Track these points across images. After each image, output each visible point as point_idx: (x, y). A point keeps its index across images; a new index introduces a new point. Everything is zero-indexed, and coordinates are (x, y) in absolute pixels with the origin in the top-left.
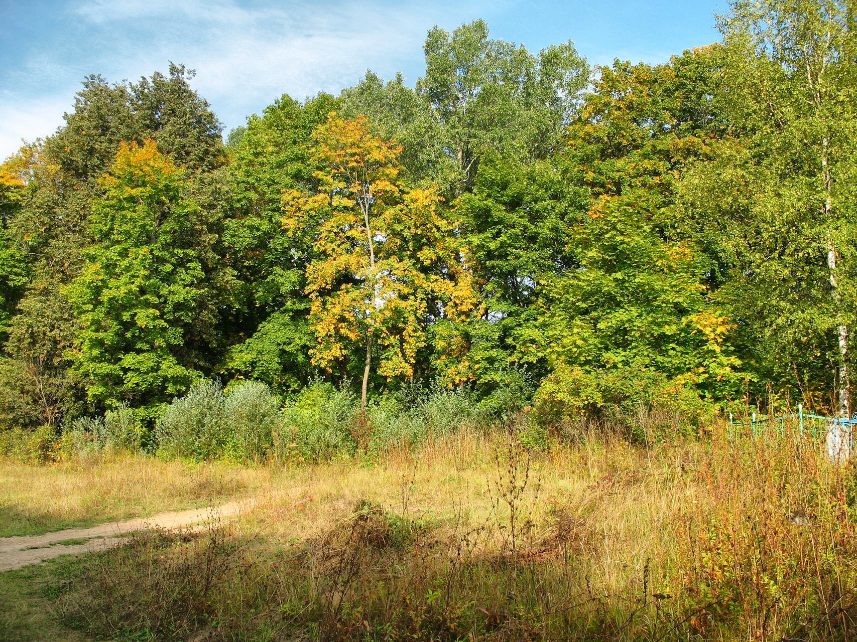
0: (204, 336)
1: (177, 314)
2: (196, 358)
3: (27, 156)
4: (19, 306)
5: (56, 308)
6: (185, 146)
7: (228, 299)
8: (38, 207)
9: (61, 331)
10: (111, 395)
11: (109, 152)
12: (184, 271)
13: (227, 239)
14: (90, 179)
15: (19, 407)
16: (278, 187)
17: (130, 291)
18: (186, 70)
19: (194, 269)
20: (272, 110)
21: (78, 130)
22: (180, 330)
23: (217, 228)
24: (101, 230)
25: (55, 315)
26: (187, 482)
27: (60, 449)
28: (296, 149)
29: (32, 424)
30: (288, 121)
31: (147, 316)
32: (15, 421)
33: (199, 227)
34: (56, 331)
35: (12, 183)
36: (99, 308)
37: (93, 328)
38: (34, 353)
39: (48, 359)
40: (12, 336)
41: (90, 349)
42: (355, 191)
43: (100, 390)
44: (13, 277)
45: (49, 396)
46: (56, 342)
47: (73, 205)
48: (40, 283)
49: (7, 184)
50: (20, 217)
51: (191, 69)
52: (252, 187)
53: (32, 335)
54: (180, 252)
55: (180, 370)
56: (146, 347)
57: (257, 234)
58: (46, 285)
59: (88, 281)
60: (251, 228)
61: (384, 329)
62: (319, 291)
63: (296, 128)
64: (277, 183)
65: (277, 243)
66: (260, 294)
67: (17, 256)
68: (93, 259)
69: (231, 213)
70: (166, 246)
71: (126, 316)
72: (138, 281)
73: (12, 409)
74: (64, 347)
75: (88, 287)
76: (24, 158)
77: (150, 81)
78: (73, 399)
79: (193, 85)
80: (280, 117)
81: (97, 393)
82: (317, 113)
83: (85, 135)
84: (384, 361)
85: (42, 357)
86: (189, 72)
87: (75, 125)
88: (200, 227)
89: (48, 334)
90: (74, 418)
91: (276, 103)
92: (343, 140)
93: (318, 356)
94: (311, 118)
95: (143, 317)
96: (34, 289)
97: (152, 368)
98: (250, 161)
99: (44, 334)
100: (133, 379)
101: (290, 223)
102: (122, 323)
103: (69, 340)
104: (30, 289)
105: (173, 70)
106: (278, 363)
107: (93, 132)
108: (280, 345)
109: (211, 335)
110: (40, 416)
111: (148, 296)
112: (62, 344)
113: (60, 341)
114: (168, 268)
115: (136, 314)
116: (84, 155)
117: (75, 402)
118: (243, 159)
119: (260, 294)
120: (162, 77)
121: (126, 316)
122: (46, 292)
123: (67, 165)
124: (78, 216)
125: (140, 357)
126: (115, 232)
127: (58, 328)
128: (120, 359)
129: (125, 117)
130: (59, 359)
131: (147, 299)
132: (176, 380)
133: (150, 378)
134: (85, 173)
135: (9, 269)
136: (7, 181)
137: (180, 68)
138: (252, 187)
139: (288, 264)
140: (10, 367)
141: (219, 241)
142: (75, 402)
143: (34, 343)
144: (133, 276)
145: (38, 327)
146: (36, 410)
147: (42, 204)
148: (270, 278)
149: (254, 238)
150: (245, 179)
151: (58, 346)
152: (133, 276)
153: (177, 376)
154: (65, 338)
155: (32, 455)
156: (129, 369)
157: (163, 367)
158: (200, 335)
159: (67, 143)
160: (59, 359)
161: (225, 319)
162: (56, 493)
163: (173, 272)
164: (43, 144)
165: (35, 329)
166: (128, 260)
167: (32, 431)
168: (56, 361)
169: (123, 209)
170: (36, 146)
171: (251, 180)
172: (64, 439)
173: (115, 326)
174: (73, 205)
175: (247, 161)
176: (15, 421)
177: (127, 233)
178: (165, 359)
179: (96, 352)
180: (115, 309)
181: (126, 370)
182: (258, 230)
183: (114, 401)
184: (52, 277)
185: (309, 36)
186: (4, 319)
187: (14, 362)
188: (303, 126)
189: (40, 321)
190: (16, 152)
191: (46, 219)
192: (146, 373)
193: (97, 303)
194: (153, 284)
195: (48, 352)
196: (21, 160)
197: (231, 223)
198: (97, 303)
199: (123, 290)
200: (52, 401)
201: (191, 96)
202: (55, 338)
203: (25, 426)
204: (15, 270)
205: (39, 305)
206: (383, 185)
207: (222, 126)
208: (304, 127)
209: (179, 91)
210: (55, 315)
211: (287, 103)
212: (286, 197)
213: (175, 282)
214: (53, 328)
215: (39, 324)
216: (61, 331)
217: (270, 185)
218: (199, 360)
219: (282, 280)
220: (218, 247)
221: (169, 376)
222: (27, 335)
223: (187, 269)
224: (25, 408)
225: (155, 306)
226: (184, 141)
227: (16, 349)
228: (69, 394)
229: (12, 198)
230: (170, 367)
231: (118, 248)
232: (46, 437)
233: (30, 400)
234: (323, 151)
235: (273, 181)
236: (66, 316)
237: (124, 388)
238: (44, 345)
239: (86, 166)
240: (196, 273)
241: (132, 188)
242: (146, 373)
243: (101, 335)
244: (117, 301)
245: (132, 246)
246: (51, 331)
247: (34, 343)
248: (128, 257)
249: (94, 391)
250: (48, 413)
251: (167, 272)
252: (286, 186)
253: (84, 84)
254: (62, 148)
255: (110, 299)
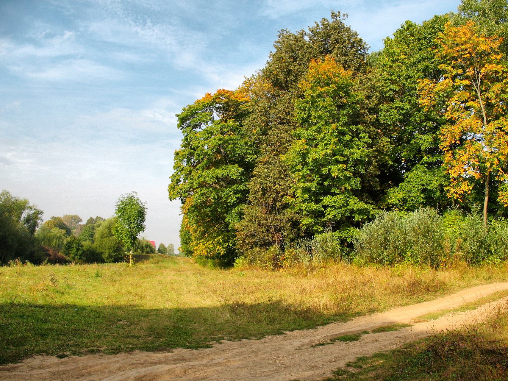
0: (371, 183)
1: (356, 168)
2: (366, 198)
3: (248, 86)
4: (254, 173)
5: (276, 171)
6: (347, 61)
7: (385, 158)
8: (260, 112)
9: (280, 185)
10: (317, 224)
11: (299, 72)
12: (357, 140)
13: (382, 118)
14: (290, 89)
15: (258, 234)
16: (413, 79)
17: (327, 153)
18: (341, 15)
19: (364, 138)
20: (399, 32)
21: (280, 59)
22: (359, 179)
23: (374, 111)
24: (302, 117)
25: (275, 176)
26: (403, 283)
27: (284, 260)
28: (422, 53)
29: (267, 244)
30: (411, 38)
31: (339, 170)
32: (256, 244)
33: (362, 112)
34: (277, 186)
35: (242, 100)
36: (306, 167)
37: (302, 181)
38: (265, 200)
39: (273, 204)
40: (252, 190)
41: (302, 194)
42: (470, 74)
43: (310, 221)
44: (247, 156)
45: (275, 227)
46: (277, 193)
47: (281, 106)
48: (264, 158)
49: (240, 101)
50: (249, 119)
51: (345, 13)
52: (393, 82)
53: (263, 189)
54: (354, 128)
55: (362, 205)
56: (338, 191)
57: (403, 112)
58: (267, 159)
59: (298, 150)
60: (398, 108)
61: (500, 169)
62: (450, 146)
63: (419, 40)
64: (412, 77)
65: (417, 117)
66: (405, 153)
67: (249, 143)
68: (299, 137)
69: (383, 99)
70: (346, 124)
71: (325, 171)
72: (332, 146)
73: (253, 235)
74: (282, 196)
75: (298, 154)
76: (246, 87)
77: (320, 24)
78: (291, 228)
79: (347, 23)
80: (407, 36)
81: (308, 223)
82: (433, 27)
83: (284, 62)
84: (501, 192)
85: (270, 203)
86: (344, 15)
87: (277, 58)
88: (363, 111)
89: (273, 187)
90: (292, 240)
91: (402, 27)
92: (458, 40)
93: (452, 191)
94: (430, 31)
95: (335, 170)
96: (260, 162)
97: (343, 205)
98: (390, 66)
99: (270, 188)
100: (331, 212)
101: (425, 102)
102: (321, 176)
103: (285, 191)
104: (257, 163)
105: (334, 16)
106: (423, 198)
107: (289, 60)
108: (424, 185)
109: (376, 182)
110: (271, 240)
111: (337, 157)
112: (281, 194)
113: (280, 192)
114: (348, 137)
115: (330, 169)
116: (285, 75)
117: (291, 230)
118: (385, 65)
119: (405, 153)
120: (327, 21)
121: (325, 171)
122: (267, 163)
123: (276, 83)
124: (285, 113)
125: (335, 198)
126: (312, 117)
127: (278, 184)
128: (322, 200)
129: (308, 47)
130: (280, 203)
131: (337, 158)
132: (361, 212)
133: (342, 211)
134: (287, 86)
135: (245, 151)
136: (239, 99)
137: (338, 13)
138: (393, 82)
139: (424, 132)
140: (250, 211)
141: (377, 120)
142: (291, 230)
143: (264, 195)
144: (326, 144)
145: (266, 184)
146: (268, 236)
147: (262, 109)
148: (413, 141)
149: (400, 114)
150: (390, 77)
151: (279, 195)
152: (326, 144)
153: (361, 209)
154: (283, 190)
155: (268, 264)
156: (328, 206)
157: (350, 203)
158: (368, 182)
159: (274, 69)
160: (280, 203)
161: (382, 172)
162: (303, 291)
163: (351, 141)
164: (256, 78)
165: (265, 185)
166: (322, 134)
167: (267, 249)
168: (278, 204)
169: (315, 102)
170: (252, 80)
171: (393, 77)
172: (286, 254)
173: (317, 178)
174: (281, 106)
175: (388, 66)
176: (256, 244)
177: (320, 117)
178: (351, 198)
179: (306, 196)
180: (317, 166)
181: (325, 207)
182: (403, 109)
183: (319, 227)
184: (270, 153)
185: (397, 5)
186: (244, 182)
187: (252, 207)
188: (424, 38)
189: (267, 180)
190: (241, 85)
191: (264, 118)
192: (340, 208)
193: (305, 164)
194: (339, 149)
195: (273, 199)
196: (244, 88)
197: (384, 107)
198: (305, 164)
199: (322, 153)
200: (278, 230)
201: (347, 30)
202: (277, 190)
203: (261, 246)
204: (248, 151)
205: (266, 170)
206: (489, 67)
207: (368, 46)
208: (425, 38)
209: (339, 28)
210: (275, 176)
211: (409, 26)
212: (420, 85)
213: (353, 147)
214: (275, 184)
215: (267, 182)
216: (280, 185)
217: (407, 79)
218: (369, 199)
219: (421, 142)
220: (376, 124)
221: (355, 209)
222: (260, 189)
223: (359, 138)
224: (262, 235)
225: (344, 162)
226: (346, 58)
227: (254, 198)
228: (288, 225)
229: (243, 109)
230: (355, 203)
231: (314, 128)
232: (276, 252)
233: (264, 230)
234: (444, 50)
235: (409, 76)
236: (282, 176)
237: (325, 219)
238: (270, 195)
239: (287, 81)
240: (365, 140)
241: (322, 87)
242: (340, 208)
243: (309, 185)
244: (318, 162)
245: (324, 125)
246: (274, 186)
247: (264, 195)
248: (322, 132)
249: (307, 221)
250: (276, 238)
251: (348, 141)
252: (419, 78)
253: (278, 36)
254: (271, 72)
255: (314, 160)
